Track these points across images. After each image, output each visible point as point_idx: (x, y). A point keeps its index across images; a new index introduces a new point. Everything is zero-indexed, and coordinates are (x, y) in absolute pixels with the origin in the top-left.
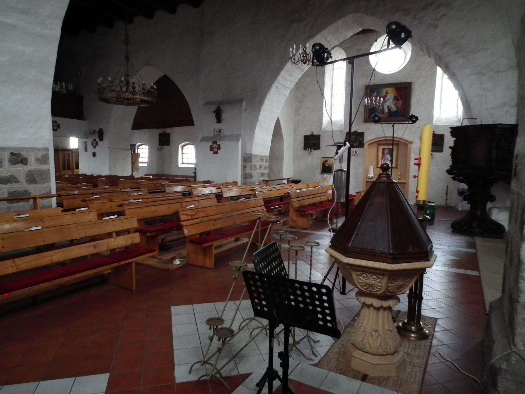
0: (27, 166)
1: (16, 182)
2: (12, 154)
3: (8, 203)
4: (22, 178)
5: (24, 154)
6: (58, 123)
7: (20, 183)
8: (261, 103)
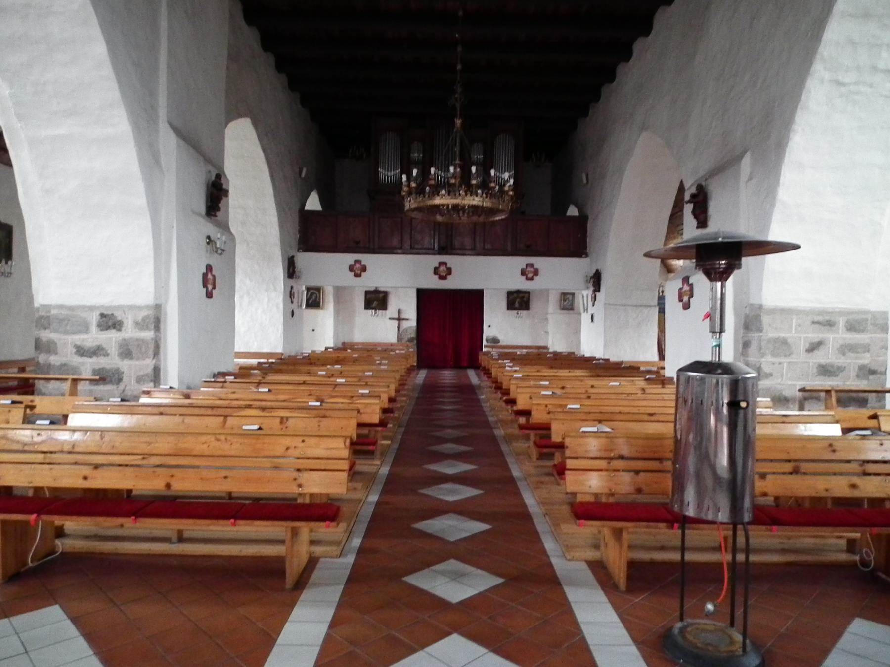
0: (120, 332)
1: (105, 356)
2: (102, 315)
3: (91, 384)
4: (113, 349)
5: (119, 315)
6: (535, 267)
7: (110, 357)
8: (781, 147)
